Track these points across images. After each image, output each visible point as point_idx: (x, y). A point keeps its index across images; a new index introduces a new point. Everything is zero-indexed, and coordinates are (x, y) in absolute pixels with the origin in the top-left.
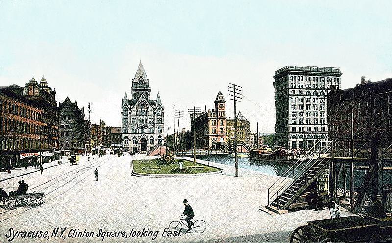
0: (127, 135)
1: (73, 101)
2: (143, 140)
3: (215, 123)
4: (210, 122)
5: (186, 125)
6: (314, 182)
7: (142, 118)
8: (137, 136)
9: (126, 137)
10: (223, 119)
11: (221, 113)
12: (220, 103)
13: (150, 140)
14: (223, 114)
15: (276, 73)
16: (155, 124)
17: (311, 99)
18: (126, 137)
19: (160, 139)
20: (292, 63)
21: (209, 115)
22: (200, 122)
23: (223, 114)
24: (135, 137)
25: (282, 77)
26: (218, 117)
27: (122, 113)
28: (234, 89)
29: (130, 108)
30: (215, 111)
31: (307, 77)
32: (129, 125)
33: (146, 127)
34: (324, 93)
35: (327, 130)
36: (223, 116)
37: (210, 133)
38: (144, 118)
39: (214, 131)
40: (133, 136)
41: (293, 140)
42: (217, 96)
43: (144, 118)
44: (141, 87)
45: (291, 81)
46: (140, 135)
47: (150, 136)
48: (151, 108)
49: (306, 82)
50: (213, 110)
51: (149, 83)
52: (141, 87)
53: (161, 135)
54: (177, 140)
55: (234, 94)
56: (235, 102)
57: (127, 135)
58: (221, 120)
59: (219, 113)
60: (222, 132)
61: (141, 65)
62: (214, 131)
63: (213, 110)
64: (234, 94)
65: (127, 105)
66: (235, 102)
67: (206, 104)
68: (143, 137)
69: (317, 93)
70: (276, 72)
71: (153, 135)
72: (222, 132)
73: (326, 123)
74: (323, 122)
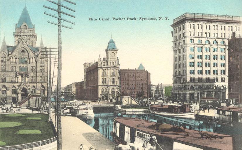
2: (24, 90)
3: (106, 73)
4: (100, 71)
5: (80, 77)
6: (35, 140)
7: (22, 65)
20: (191, 10)
22: (91, 71)
24: (14, 86)
28: (59, 12)
30: (106, 60)
32: (8, 73)
33: (26, 75)
41: (190, 92)
50: (104, 58)
52: (111, 42)
54: (74, 90)
56: (60, 31)
60: (113, 82)
63: (104, 58)
66: (60, 31)
68: (23, 86)
70: (174, 20)
72: (113, 82)
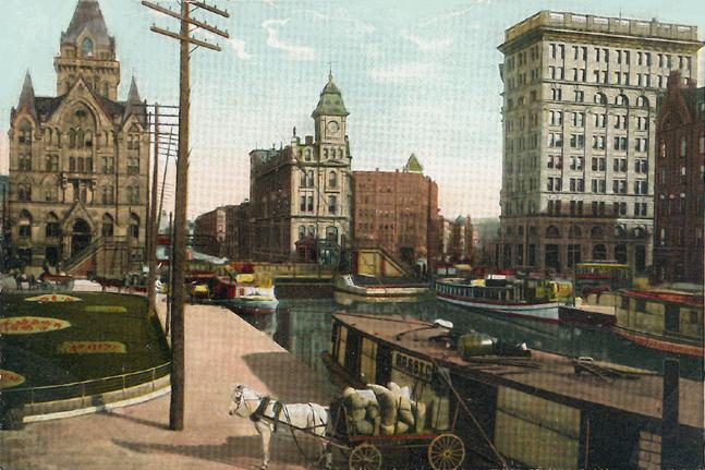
0: (30, 207)
1: (501, 58)
4: (297, 175)
7: (77, 153)
11: (329, 147)
15: (507, 36)
17: (610, 117)
22: (271, 172)
25: (525, 43)
26: (323, 160)
30: (315, 144)
31: (576, 48)
34: (646, 100)
35: (651, 211)
38: (85, 153)
43: (85, 153)
45: (556, 59)
49: (594, 62)
55: (185, 29)
57: (30, 207)
60: (332, 209)
63: (309, 139)
64: (185, 29)
69: (604, 99)
72: (332, 209)
73: (651, 191)
74: (643, 188)
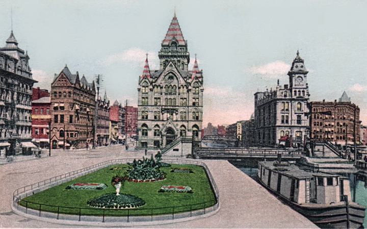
2: (170, 130)
4: (280, 106)
5: (247, 112)
8: (160, 123)
9: (144, 125)
10: (302, 100)
12: (297, 76)
13: (179, 131)
14: (301, 93)
16: (188, 107)
18: (144, 125)
19: (145, 128)
21: (278, 93)
22: (266, 104)
23: (301, 93)
24: (157, 125)
25: (215, 200)
27: (139, 90)
29: (151, 83)
30: (289, 88)
36: (302, 95)
37: (279, 123)
38: (172, 97)
39: (285, 120)
40: (155, 123)
42: (293, 64)
43: (172, 97)
44: (174, 50)
46: (165, 123)
47: (180, 124)
48: (182, 82)
51: (186, 46)
53: (197, 123)
58: (297, 102)
59: (295, 91)
61: (175, 25)
62: (285, 120)
65: (149, 79)
67: (276, 73)
71: (185, 124)
